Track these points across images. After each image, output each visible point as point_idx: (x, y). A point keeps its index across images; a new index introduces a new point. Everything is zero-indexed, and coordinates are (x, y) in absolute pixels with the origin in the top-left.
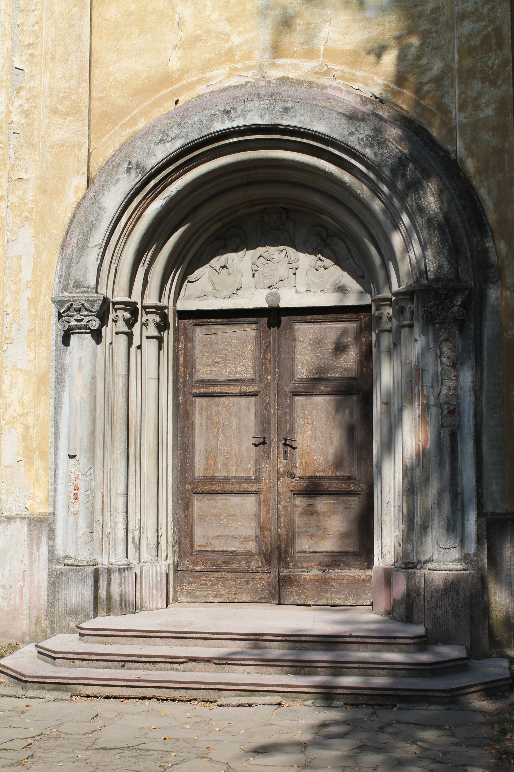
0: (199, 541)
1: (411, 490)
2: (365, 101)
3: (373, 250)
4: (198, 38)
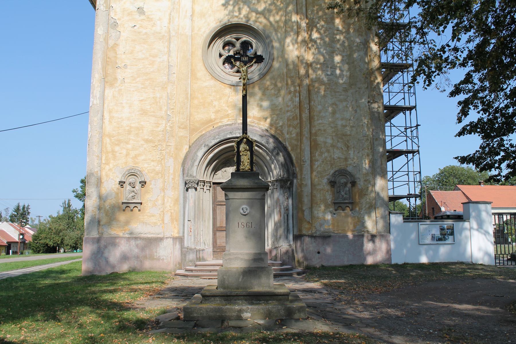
0: (218, 243)
1: (276, 229)
2: (263, 130)
3: (266, 169)
4: (219, 111)
